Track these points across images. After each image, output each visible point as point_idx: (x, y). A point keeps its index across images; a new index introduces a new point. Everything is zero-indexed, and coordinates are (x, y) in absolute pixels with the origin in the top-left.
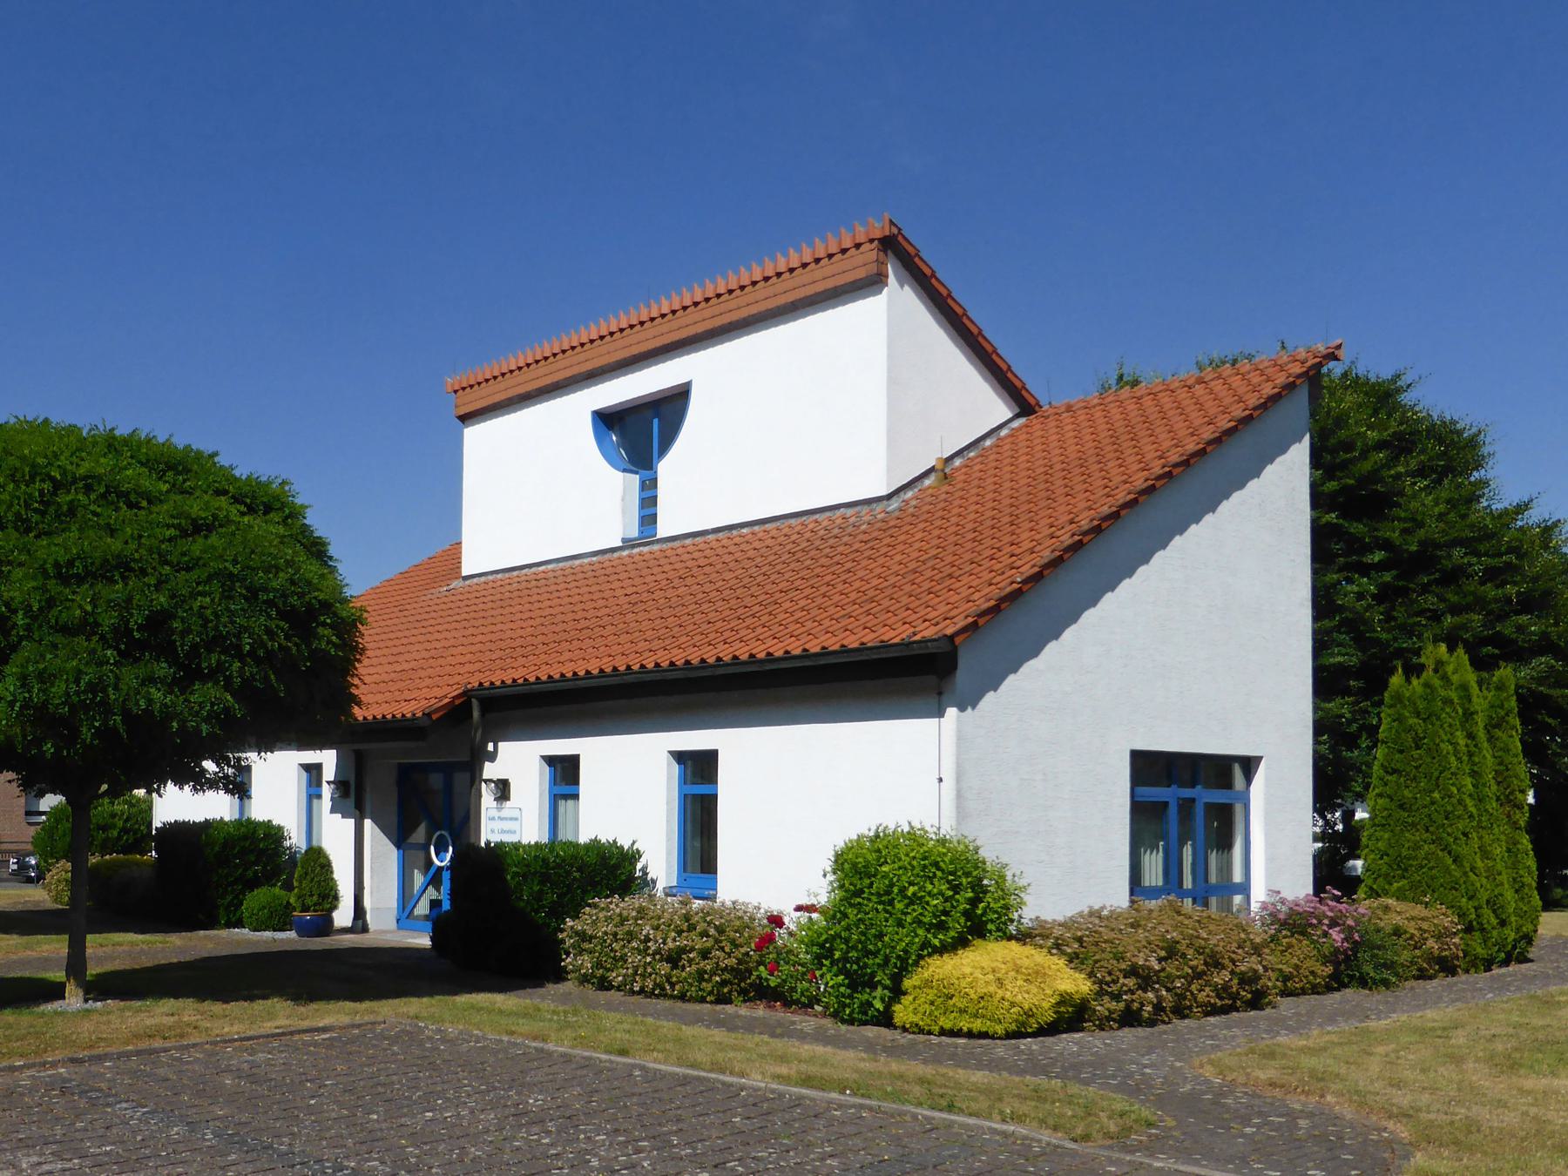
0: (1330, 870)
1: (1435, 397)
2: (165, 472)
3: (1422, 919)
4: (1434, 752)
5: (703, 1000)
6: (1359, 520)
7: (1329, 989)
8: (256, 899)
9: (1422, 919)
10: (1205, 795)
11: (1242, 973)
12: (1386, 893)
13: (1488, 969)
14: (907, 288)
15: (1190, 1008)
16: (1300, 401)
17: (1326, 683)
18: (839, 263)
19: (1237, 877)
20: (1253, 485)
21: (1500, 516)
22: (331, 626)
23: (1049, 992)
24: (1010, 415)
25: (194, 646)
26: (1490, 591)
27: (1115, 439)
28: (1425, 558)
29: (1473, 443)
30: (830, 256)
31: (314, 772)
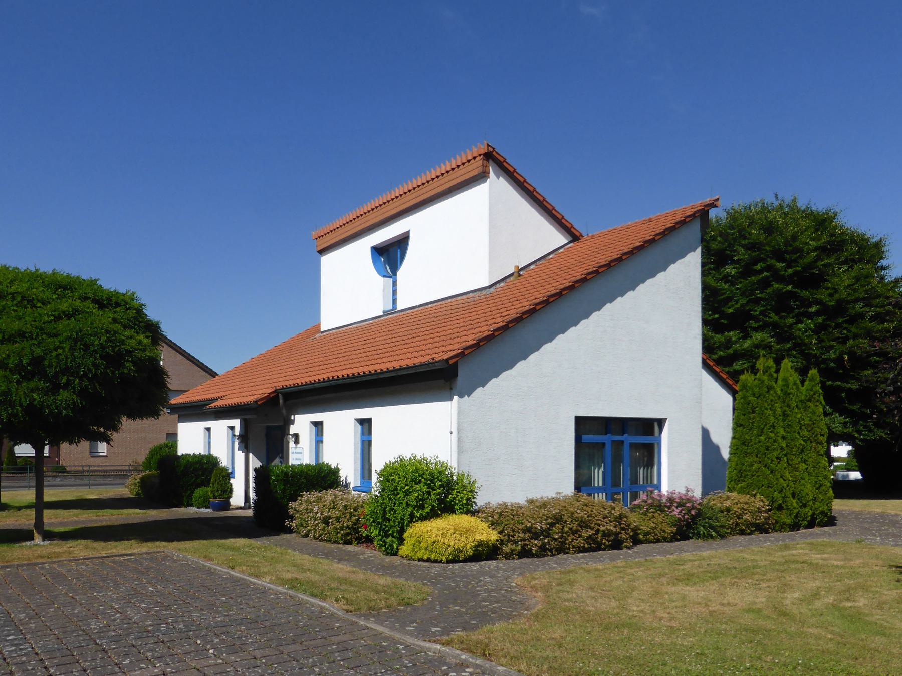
2: (57, 289)
5: (335, 542)
6: (807, 290)
8: (199, 492)
11: (603, 531)
14: (501, 178)
15: (569, 549)
16: (695, 228)
20: (661, 276)
25: (56, 373)
28: (841, 308)
29: (878, 246)
30: (463, 164)
31: (366, 425)
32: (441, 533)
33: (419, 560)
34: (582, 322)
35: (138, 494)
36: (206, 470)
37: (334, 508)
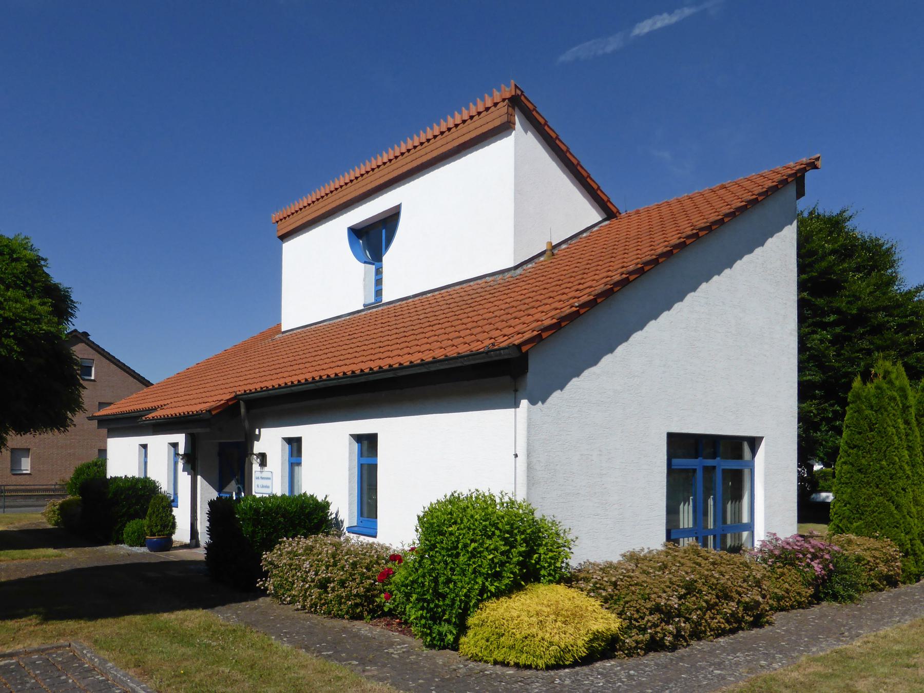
0: (809, 510)
1: (864, 226)
3: (875, 549)
4: (883, 433)
6: (821, 297)
7: (810, 604)
8: (132, 526)
9: (875, 549)
10: (724, 464)
11: (746, 603)
12: (848, 530)
13: (918, 580)
14: (529, 133)
17: (805, 391)
18: (485, 117)
19: (745, 519)
20: (758, 251)
21: (906, 293)
22: (14, 337)
23: (583, 632)
24: (601, 219)
26: (901, 338)
27: (662, 223)
28: (861, 318)
31: (295, 445)
32: (534, 619)
33: (496, 663)
34: (676, 306)
35: (57, 523)
36: (143, 498)
37: (335, 565)
